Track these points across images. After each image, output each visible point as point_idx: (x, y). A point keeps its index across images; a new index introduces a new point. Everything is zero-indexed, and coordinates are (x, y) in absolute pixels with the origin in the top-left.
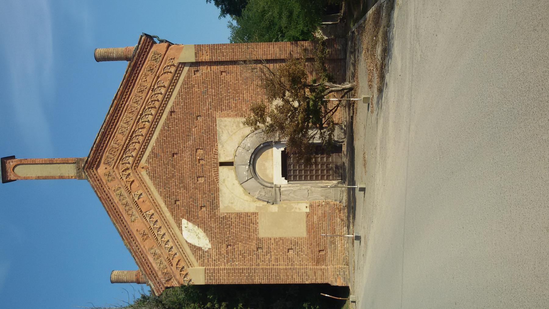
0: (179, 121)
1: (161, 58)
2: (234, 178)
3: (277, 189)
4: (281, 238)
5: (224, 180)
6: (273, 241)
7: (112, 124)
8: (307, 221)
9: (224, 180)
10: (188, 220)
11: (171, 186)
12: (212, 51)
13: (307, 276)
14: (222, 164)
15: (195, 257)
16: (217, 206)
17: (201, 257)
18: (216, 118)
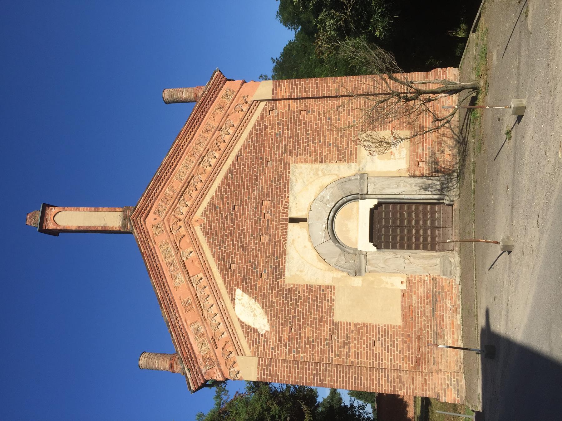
1: (233, 96)
3: (362, 257)
4: (364, 324)
5: (293, 240)
6: (353, 328)
8: (402, 302)
10: (243, 291)
11: (228, 246)
12: (292, 87)
13: (400, 383)
16: (282, 275)
17: (254, 342)
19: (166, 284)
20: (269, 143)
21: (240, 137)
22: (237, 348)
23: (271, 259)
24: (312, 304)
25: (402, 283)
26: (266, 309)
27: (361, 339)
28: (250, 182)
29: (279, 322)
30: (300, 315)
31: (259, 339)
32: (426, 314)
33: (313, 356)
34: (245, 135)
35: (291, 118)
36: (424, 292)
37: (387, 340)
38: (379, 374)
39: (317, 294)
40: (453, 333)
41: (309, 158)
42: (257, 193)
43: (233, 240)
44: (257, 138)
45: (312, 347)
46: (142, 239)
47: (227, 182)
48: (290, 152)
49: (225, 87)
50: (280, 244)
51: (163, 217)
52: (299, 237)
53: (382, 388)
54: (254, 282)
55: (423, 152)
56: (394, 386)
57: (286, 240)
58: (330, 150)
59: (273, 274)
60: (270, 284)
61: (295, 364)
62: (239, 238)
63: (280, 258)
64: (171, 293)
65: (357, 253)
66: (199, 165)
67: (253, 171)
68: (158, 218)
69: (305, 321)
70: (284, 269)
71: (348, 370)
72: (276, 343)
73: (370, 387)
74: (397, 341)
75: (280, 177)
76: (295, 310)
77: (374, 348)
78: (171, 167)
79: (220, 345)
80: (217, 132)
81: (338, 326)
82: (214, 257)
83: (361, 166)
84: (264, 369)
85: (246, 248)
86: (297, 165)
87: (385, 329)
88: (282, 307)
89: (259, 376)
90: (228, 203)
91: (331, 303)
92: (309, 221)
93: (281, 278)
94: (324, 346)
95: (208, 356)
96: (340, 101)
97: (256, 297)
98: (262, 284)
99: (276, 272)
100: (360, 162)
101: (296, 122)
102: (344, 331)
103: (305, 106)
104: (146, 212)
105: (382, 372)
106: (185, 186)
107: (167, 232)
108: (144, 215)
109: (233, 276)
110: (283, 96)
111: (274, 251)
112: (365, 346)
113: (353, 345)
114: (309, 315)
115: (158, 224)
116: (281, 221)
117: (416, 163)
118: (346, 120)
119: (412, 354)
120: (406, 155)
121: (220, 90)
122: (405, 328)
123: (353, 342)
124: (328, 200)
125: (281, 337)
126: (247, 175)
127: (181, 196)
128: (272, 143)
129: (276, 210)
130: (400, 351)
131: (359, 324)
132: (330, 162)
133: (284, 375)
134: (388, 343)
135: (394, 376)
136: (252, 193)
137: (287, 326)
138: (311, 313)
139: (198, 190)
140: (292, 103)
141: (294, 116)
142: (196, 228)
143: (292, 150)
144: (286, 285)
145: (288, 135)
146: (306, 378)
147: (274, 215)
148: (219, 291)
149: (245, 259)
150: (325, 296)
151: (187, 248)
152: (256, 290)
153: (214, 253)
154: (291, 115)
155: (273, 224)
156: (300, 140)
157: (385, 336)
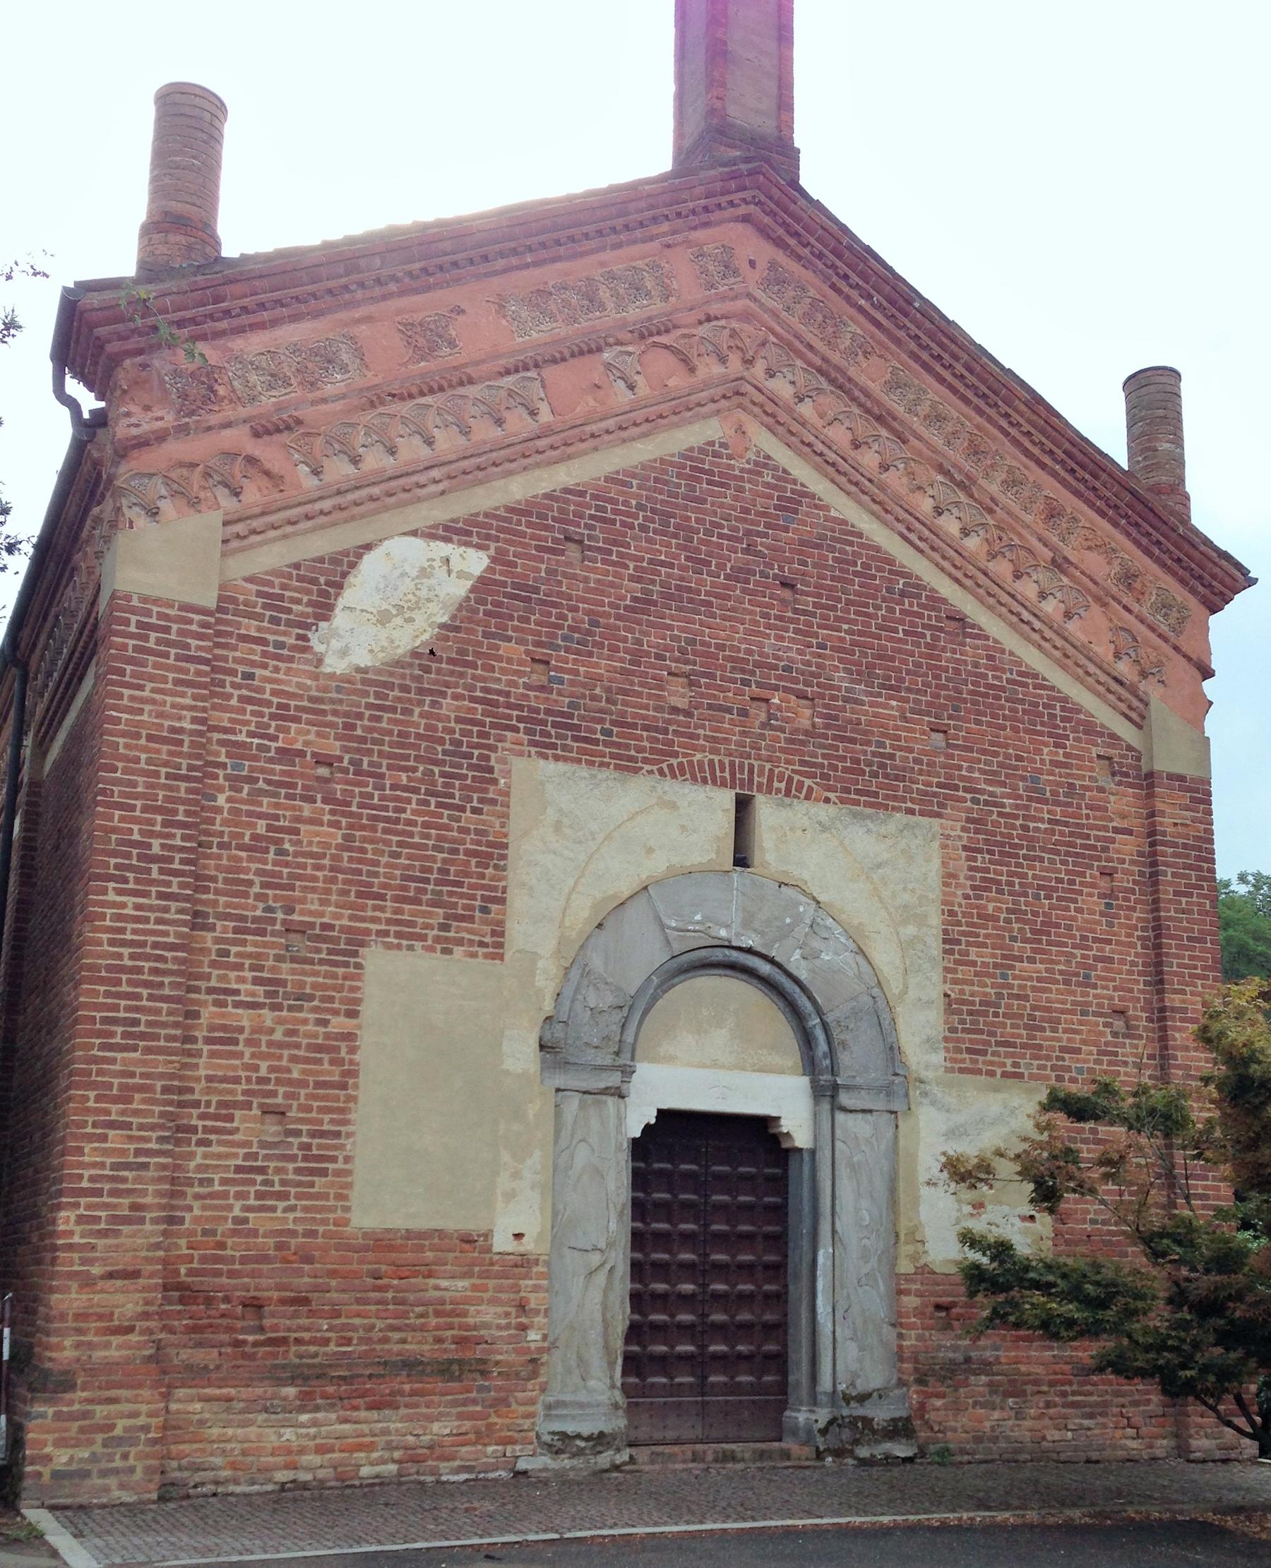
0: (927, 645)
1: (1164, 628)
2: (675, 860)
3: (614, 1079)
4: (353, 1074)
5: (674, 806)
6: (339, 1024)
7: (937, 350)
8: (441, 1233)
9: (674, 806)
10: (481, 580)
11: (649, 540)
12: (1193, 848)
13: (114, 1219)
14: (743, 806)
15: (276, 573)
16: (545, 748)
17: (274, 602)
18: (939, 815)
19: (514, 261)
20: (1006, 746)
21: (1028, 639)
22: (255, 524)
23: (601, 711)
24: (433, 859)
25: (518, 1236)
26: (411, 665)
27: (294, 1059)
28: (880, 657)
29: (360, 716)
30: (386, 809)
31: (289, 623)
32: (396, 1336)
33: (221, 846)
34: (1033, 658)
35: (1088, 837)
36: (486, 1326)
37: (291, 1166)
38: (153, 1127)
39: (471, 887)
40: (320, 1450)
41: (959, 893)
42: (840, 678)
43: (672, 566)
44: (1022, 702)
47: (879, 569)
48: (976, 823)
50: (661, 752)
51: (759, 294)
53: (91, 1138)
54: (515, 629)
56: (98, 1193)
57: (674, 776)
58: (988, 975)
59: (549, 712)
60: (508, 694)
61: (191, 768)
62: (679, 588)
63: (606, 744)
65: (624, 1060)
67: (916, 674)
69: (363, 828)
70: (565, 759)
71: (167, 992)
72: (274, 693)
73: (94, 1085)
74: (286, 1210)
75: (897, 778)
76: (406, 789)
77: (256, 1111)
79: (269, 453)
80: (1048, 554)
81: (346, 965)
82: (607, 479)
83: (936, 1091)
84: (167, 630)
85: (643, 612)
86: (936, 844)
87: (333, 1159)
88: (418, 736)
89: (135, 602)
90: (805, 564)
91: (437, 939)
92: (738, 875)
93: (533, 743)
94: (259, 897)
95: (222, 391)
97: (457, 629)
98: (510, 661)
99: (555, 725)
101: (1077, 855)
102: (324, 987)
103: (1127, 890)
104: (780, 231)
105: (161, 1140)
109: (538, 548)
111: (634, 726)
112: (263, 1072)
113: (269, 1023)
114: (387, 843)
115: (736, 272)
118: (1084, 1042)
119: (232, 1274)
121: (1183, 582)
123: (280, 1021)
125: (297, 720)
126: (900, 651)
127: (832, 381)
128: (1007, 756)
129: (782, 750)
130: (246, 1221)
131: (353, 1050)
132: (946, 970)
133: (141, 711)
134: (278, 1171)
135: (144, 1193)
136: (841, 660)
137: (346, 750)
139: (852, 453)
141: (1094, 848)
142: (714, 422)
143: (986, 832)
144: (503, 761)
145: (1034, 819)
146: (133, 808)
147: (762, 737)
148: (481, 482)
149: (602, 604)
150: (462, 918)
151: (658, 373)
152: (486, 635)
153: (624, 483)
154: (1098, 838)
156: (1019, 865)
157: (306, 1158)
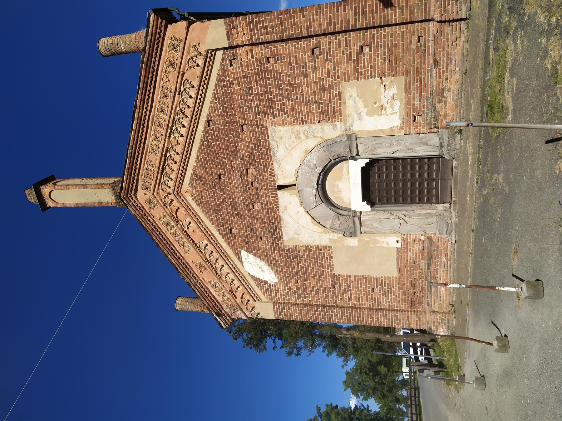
1: (182, 46)
3: (356, 219)
4: (363, 276)
5: (286, 207)
6: (352, 279)
8: (397, 259)
12: (250, 26)
16: (280, 238)
19: (176, 252)
27: (361, 287)
35: (258, 69)
41: (287, 119)
42: (238, 161)
43: (227, 208)
45: (318, 294)
46: (140, 215)
49: (168, 34)
51: (152, 192)
52: (290, 204)
55: (420, 104)
57: (278, 207)
58: (310, 107)
60: (271, 246)
64: (184, 259)
66: (170, 136)
68: (147, 193)
70: (282, 233)
73: (371, 323)
78: (141, 141)
79: (239, 295)
80: (177, 96)
86: (275, 128)
87: (382, 280)
91: (330, 260)
93: (280, 240)
94: (328, 293)
95: (230, 304)
96: (314, 41)
99: (275, 235)
100: (346, 120)
101: (265, 73)
103: (271, 51)
106: (163, 160)
107: (161, 205)
108: (133, 192)
110: (242, 41)
116: (269, 183)
117: (412, 118)
120: (400, 109)
122: (401, 278)
123: (353, 290)
124: (315, 165)
125: (290, 287)
129: (263, 178)
130: (396, 296)
131: (358, 276)
132: (311, 123)
137: (293, 278)
138: (313, 268)
140: (256, 49)
141: (261, 66)
147: (261, 183)
148: (226, 253)
150: (324, 255)
153: (212, 221)
154: (257, 66)
155: (262, 192)
